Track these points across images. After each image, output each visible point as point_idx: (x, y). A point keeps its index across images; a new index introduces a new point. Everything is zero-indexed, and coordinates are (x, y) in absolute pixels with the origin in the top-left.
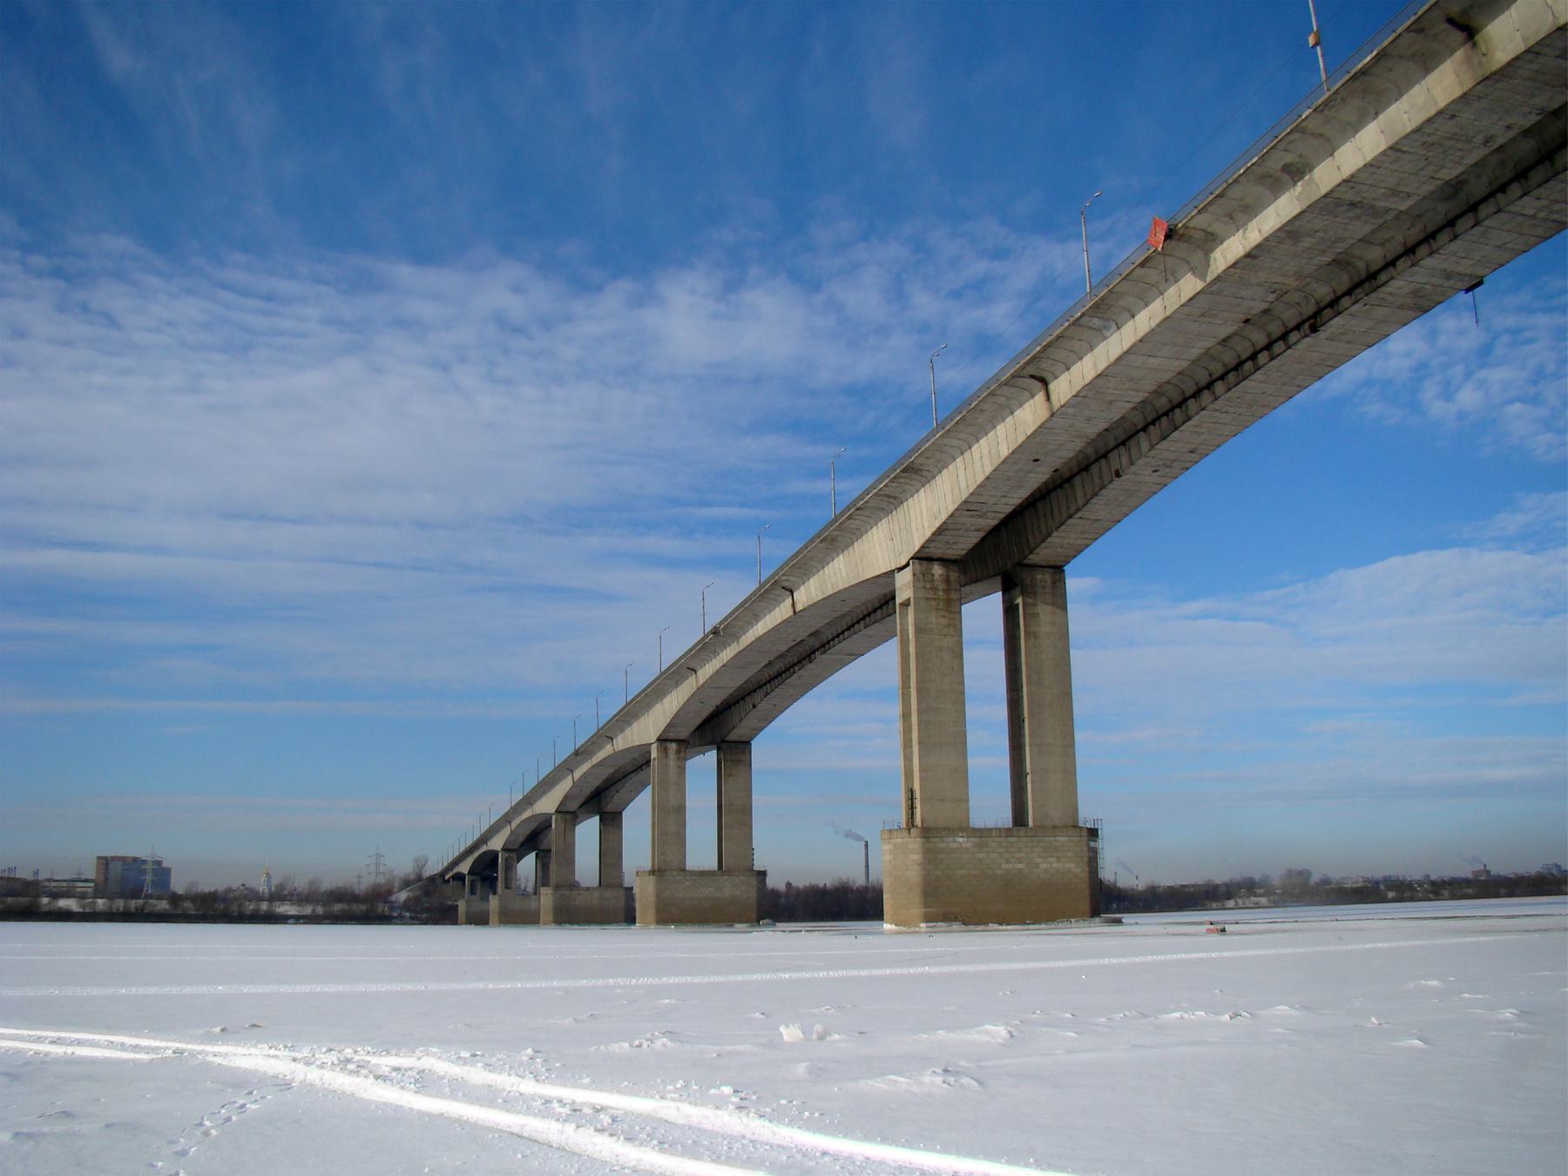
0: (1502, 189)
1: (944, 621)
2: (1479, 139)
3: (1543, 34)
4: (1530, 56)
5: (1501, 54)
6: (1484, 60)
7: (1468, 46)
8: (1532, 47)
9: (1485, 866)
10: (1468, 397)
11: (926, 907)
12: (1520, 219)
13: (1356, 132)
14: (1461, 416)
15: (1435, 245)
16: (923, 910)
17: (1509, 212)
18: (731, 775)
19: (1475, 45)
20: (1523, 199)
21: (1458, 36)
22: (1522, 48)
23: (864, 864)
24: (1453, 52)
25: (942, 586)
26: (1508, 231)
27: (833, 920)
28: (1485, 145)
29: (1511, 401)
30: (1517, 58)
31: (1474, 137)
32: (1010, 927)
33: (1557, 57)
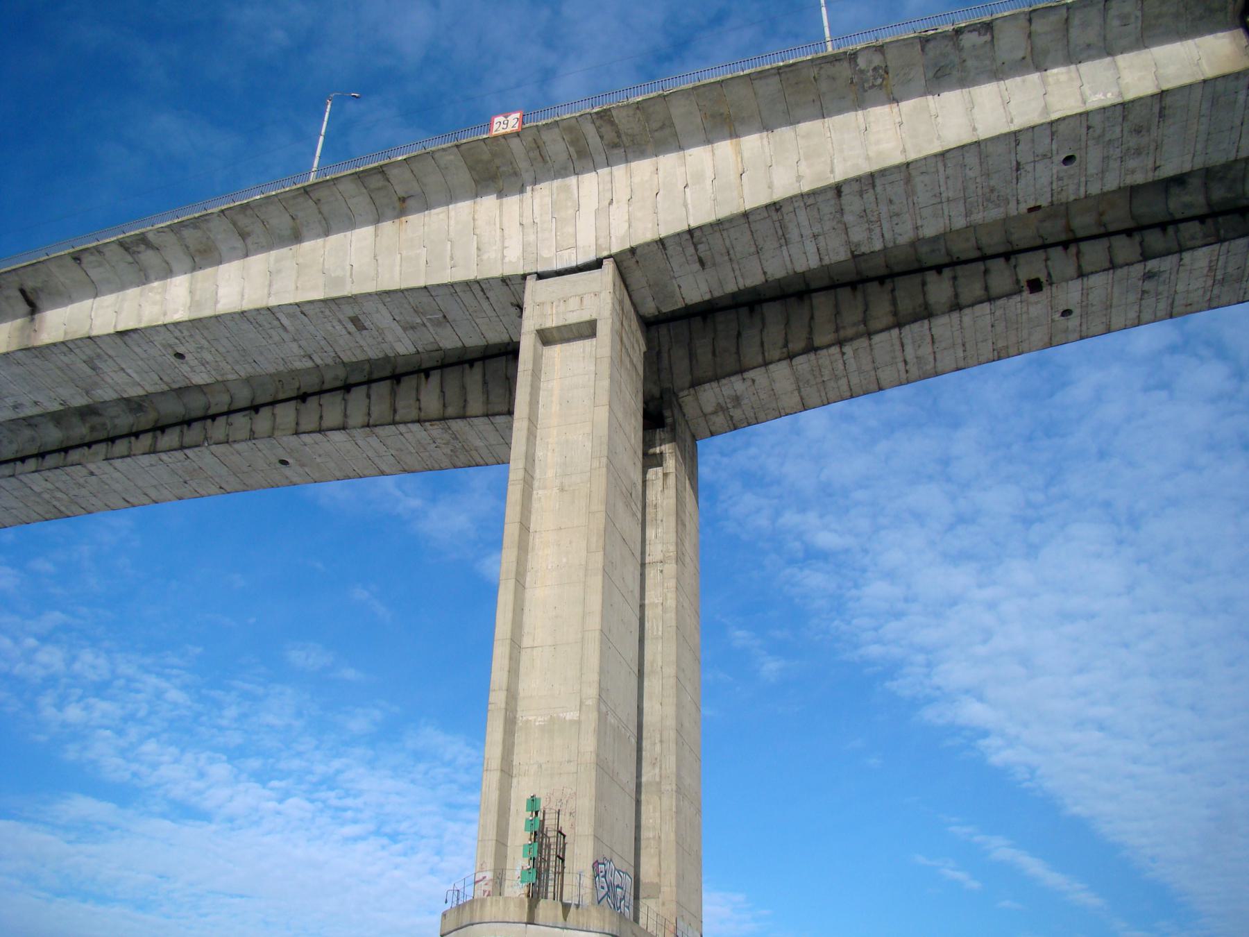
0: (23, 459)
2: (10, 401)
3: (78, 336)
4: (65, 349)
5: (46, 336)
6: (33, 334)
7: (27, 319)
8: (67, 341)
10: (74, 713)
12: (29, 491)
14: (64, 725)
17: (21, 481)
19: (33, 320)
20: (33, 474)
21: (25, 308)
22: (61, 339)
24: (15, 317)
26: (16, 498)
28: (13, 409)
29: (107, 728)
30: (54, 345)
31: (7, 397)
33: (84, 362)
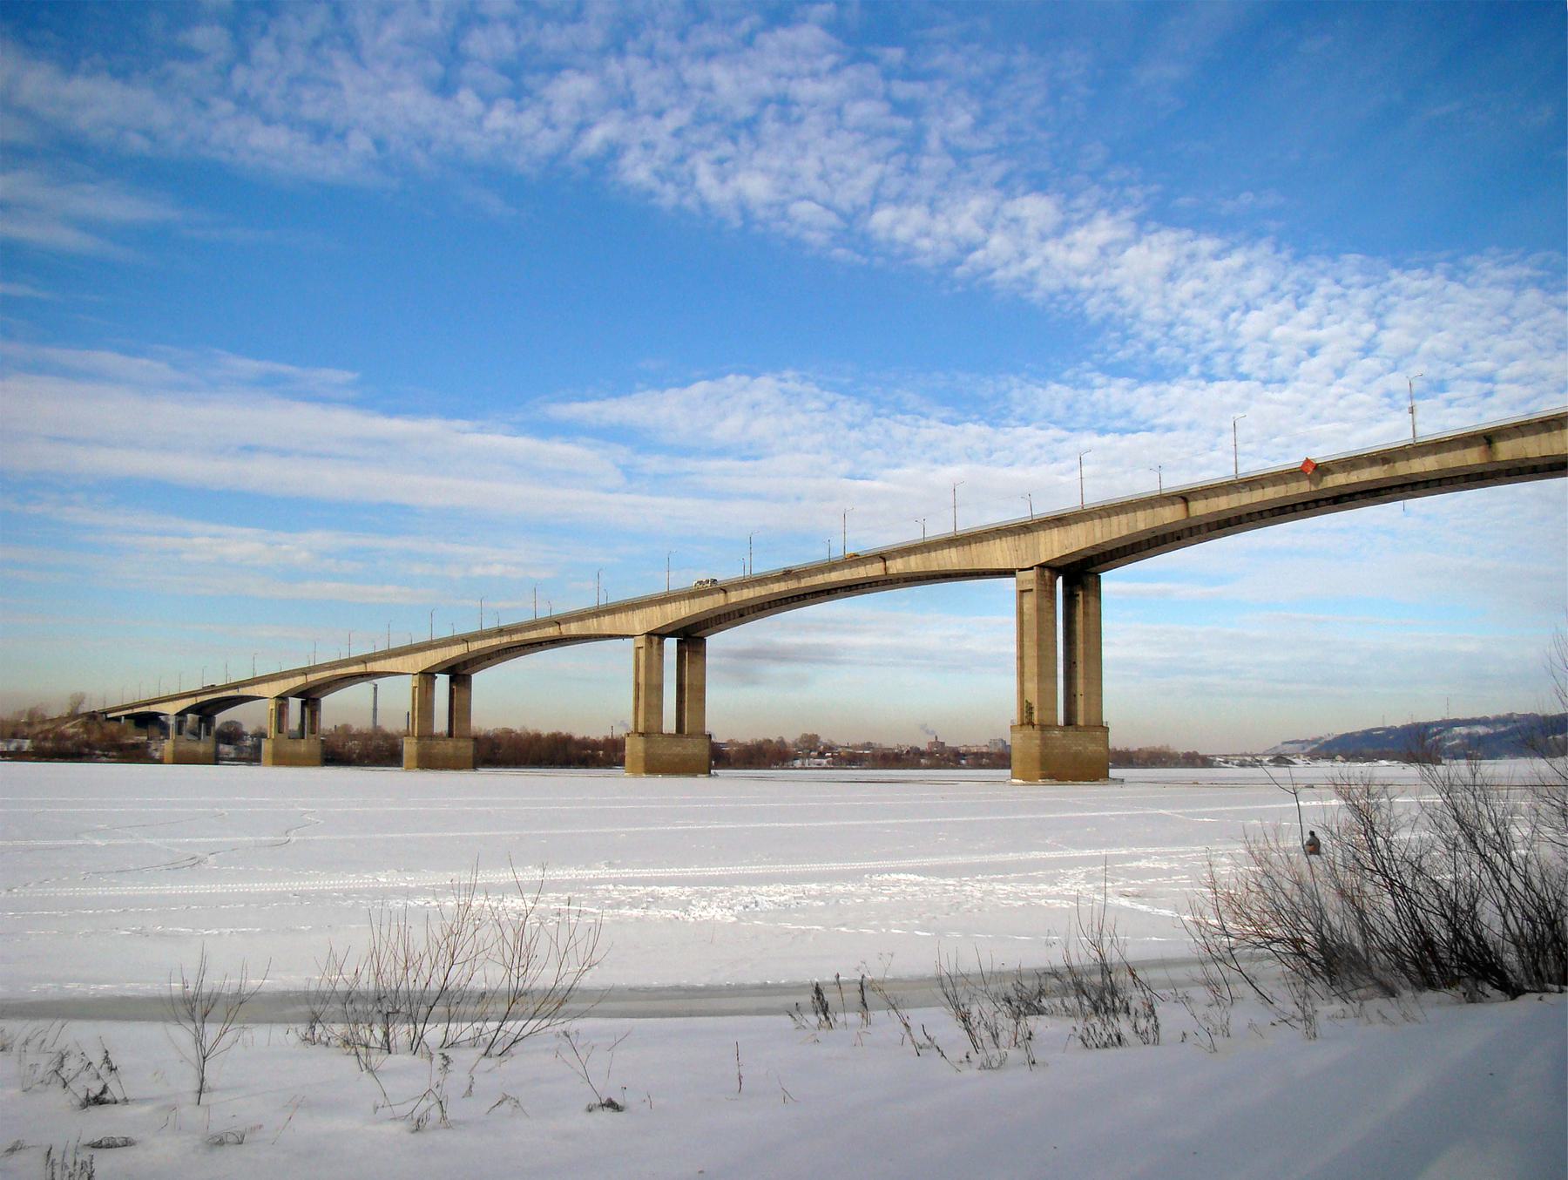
1: (1049, 604)
9: (936, 738)
11: (1042, 770)
13: (1424, 456)
15: (1415, 488)
16: (1041, 772)
18: (693, 662)
19: (1490, 447)
23: (372, 706)
25: (1048, 584)
27: (386, 766)
32: (1086, 783)
